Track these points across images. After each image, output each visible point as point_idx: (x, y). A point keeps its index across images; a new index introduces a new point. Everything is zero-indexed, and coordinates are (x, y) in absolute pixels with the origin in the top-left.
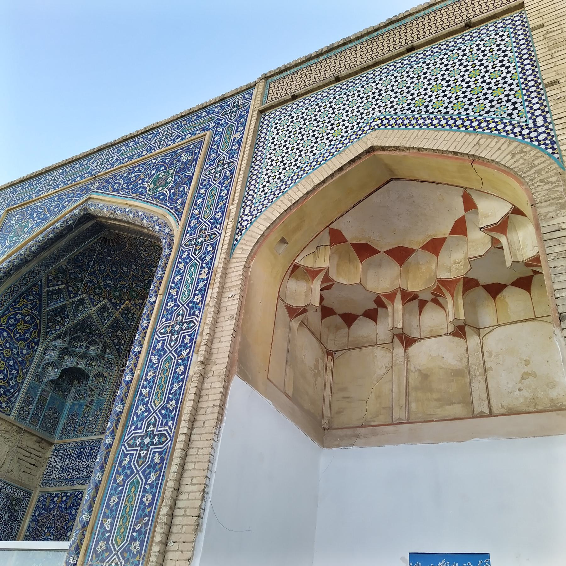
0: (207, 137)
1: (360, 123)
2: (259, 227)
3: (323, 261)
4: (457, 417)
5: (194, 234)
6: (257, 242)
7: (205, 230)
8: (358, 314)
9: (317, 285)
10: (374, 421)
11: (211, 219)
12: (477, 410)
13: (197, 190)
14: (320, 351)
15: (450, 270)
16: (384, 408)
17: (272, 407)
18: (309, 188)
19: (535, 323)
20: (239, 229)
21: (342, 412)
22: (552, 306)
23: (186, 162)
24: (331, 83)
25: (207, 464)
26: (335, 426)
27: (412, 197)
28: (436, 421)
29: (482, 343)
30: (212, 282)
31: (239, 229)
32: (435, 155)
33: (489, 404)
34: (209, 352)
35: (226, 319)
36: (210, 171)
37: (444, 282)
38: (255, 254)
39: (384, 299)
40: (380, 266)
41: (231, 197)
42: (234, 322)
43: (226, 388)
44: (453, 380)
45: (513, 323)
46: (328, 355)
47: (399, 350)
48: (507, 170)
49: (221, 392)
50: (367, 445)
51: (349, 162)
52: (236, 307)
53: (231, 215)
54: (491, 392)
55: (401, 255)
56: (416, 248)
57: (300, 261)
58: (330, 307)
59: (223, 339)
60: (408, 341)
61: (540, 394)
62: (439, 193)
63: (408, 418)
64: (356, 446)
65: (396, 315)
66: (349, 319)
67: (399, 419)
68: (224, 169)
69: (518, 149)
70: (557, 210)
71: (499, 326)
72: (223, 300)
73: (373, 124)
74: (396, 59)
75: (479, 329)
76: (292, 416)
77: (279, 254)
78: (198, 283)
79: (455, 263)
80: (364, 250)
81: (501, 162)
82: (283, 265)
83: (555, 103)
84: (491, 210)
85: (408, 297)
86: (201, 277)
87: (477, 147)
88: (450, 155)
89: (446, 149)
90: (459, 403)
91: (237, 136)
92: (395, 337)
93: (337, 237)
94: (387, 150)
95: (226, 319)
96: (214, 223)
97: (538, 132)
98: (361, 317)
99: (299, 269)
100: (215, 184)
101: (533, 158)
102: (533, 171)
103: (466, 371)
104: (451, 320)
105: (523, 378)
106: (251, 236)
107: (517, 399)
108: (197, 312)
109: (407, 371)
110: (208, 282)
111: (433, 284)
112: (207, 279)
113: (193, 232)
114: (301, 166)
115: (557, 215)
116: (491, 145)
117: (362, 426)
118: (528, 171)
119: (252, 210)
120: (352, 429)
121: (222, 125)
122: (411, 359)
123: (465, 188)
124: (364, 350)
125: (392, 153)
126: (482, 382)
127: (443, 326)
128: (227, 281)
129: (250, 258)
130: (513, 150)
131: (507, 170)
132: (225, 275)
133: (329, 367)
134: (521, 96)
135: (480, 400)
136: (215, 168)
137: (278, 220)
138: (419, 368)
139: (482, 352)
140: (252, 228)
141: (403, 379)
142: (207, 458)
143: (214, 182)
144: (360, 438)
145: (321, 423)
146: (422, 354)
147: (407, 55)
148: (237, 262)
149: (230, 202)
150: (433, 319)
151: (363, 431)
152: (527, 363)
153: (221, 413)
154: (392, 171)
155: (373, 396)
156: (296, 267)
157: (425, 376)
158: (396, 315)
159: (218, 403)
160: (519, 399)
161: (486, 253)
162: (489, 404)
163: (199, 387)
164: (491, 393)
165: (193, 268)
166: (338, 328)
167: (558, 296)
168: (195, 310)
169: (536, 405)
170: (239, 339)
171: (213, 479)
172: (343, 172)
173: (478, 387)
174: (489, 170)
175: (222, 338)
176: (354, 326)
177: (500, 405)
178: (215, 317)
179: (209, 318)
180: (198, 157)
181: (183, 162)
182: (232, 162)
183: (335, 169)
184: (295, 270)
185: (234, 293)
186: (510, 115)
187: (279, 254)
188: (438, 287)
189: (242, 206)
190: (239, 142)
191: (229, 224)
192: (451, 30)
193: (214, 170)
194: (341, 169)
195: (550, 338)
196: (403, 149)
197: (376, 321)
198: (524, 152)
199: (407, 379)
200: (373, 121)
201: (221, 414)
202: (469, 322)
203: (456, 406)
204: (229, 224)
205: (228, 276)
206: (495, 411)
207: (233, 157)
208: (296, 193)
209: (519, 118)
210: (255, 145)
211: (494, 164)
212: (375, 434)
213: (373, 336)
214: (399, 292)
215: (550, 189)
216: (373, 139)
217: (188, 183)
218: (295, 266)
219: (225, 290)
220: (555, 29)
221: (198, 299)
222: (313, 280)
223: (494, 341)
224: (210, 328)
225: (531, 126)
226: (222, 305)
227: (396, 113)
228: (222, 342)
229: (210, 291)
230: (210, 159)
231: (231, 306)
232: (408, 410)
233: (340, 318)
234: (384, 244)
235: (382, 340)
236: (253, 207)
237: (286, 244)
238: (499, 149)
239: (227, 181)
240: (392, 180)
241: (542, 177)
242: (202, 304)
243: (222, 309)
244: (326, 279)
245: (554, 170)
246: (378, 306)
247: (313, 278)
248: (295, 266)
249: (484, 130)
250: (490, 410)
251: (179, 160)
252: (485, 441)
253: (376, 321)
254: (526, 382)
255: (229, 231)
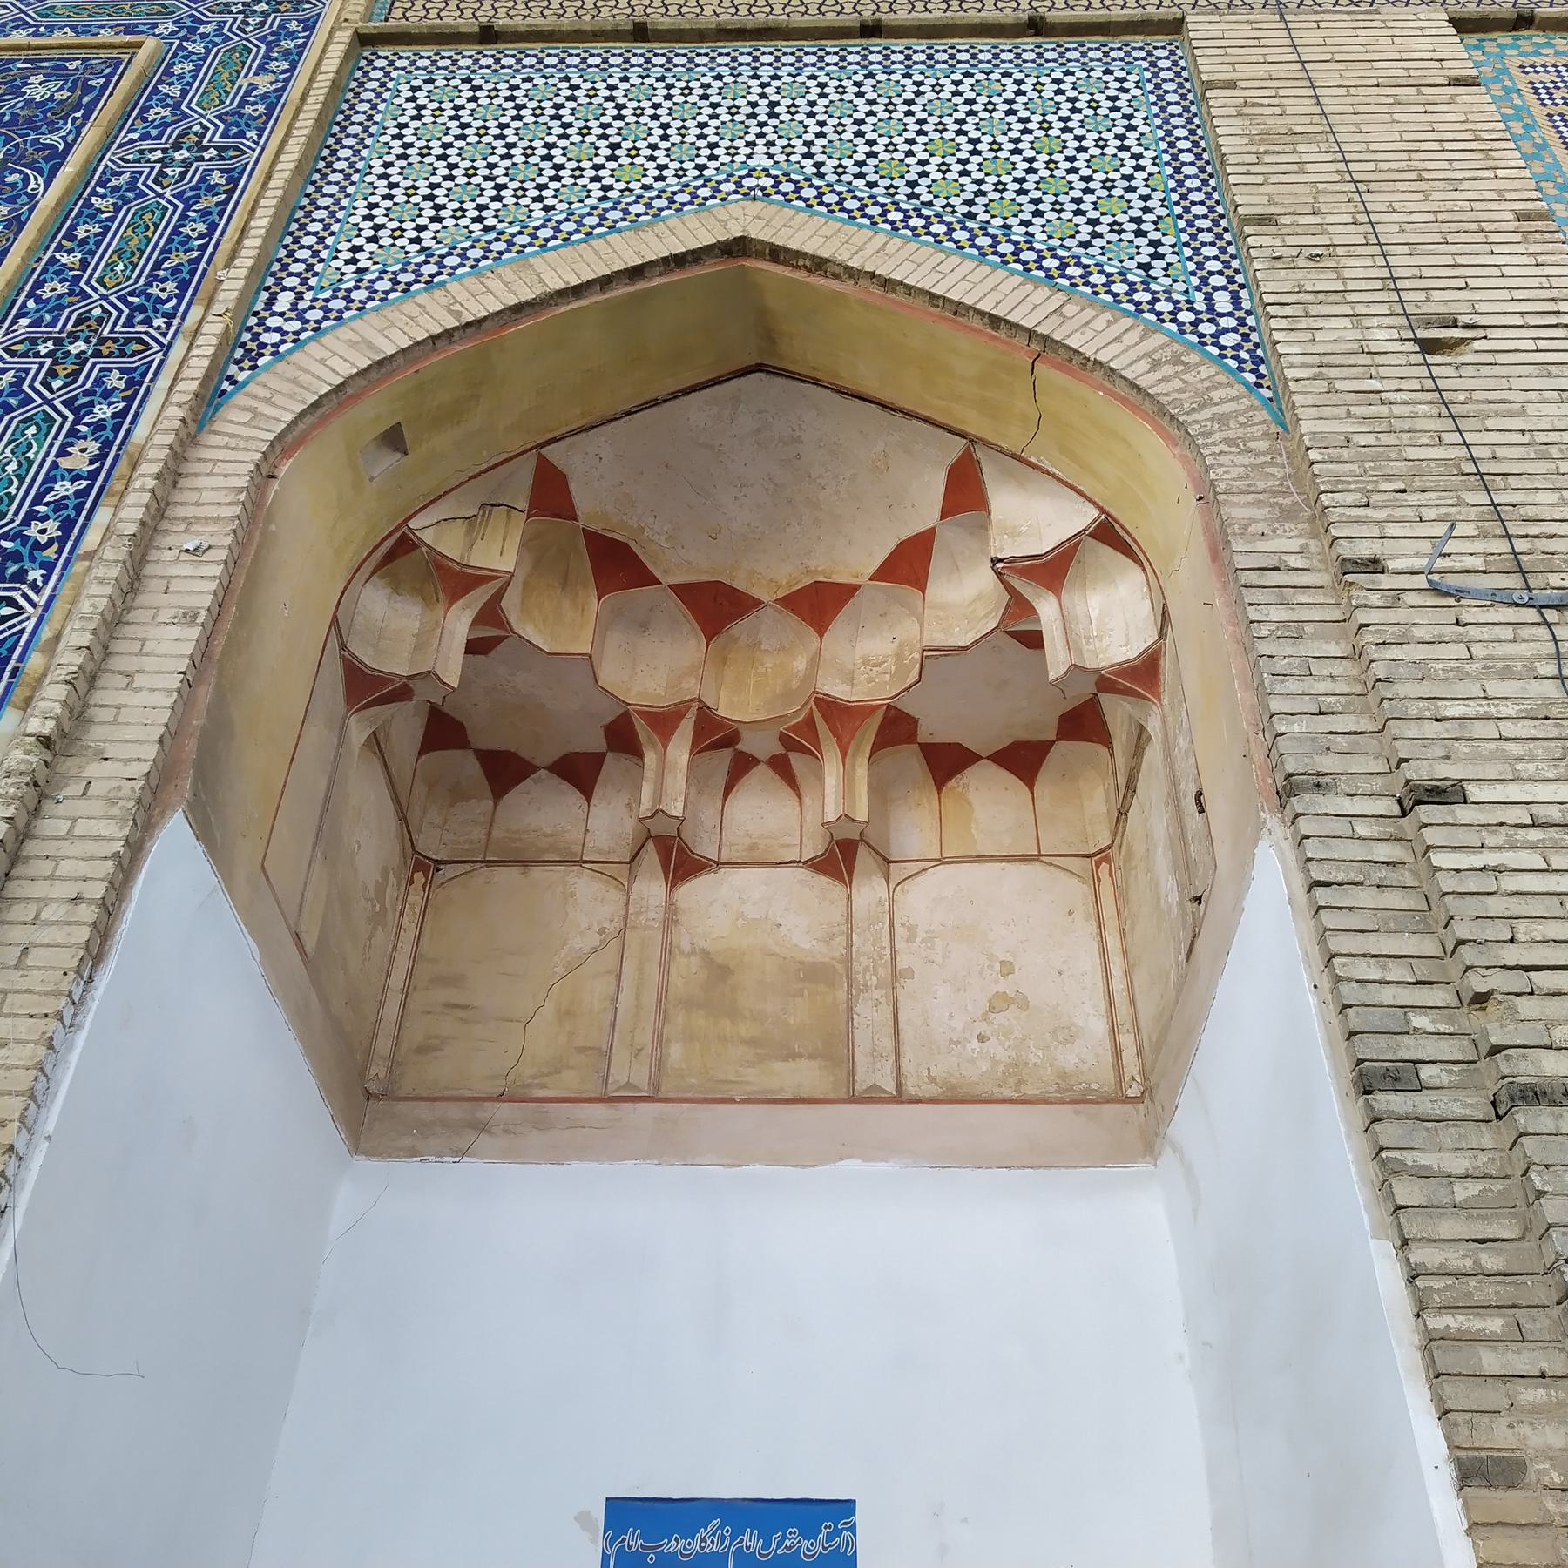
0: (142, 55)
1: (704, 167)
2: (332, 359)
3: (499, 551)
4: (804, 1095)
5: (53, 323)
6: (316, 405)
7: (99, 321)
8: (537, 762)
9: (459, 622)
10: (543, 1086)
11: (131, 294)
12: (863, 1081)
13: (79, 205)
14: (398, 848)
15: (851, 680)
16: (582, 1050)
17: (255, 968)
18: (528, 295)
19: (1035, 868)
20: (243, 349)
21: (436, 1049)
22: (1256, 759)
23: (43, 104)
24: (615, 35)
25: (18, 1103)
26: (406, 1088)
27: (798, 440)
28: (743, 1101)
29: (891, 901)
30: (116, 485)
31: (243, 349)
32: (931, 314)
33: (898, 1069)
34: (77, 715)
35: (160, 619)
36: (141, 152)
37: (831, 708)
38: (300, 441)
39: (641, 727)
40: (644, 627)
41: (226, 246)
42: (195, 632)
43: (135, 849)
44: (801, 990)
45: (980, 859)
46: (416, 870)
47: (651, 888)
48: (1136, 398)
49: (115, 856)
50: (513, 1155)
51: (665, 259)
52: (213, 585)
53: (221, 296)
54: (905, 1036)
55: (716, 608)
56: (765, 596)
57: (424, 527)
58: (459, 717)
59: (139, 681)
60: (682, 863)
61: (1034, 1056)
62: (881, 446)
63: (657, 1087)
64: (474, 1156)
65: (670, 776)
66: (504, 771)
67: (628, 1085)
68: (202, 159)
69: (1168, 352)
70: (1272, 520)
71: (943, 861)
72: (154, 555)
73: (748, 182)
74: (823, 42)
75: (889, 862)
76: (299, 1018)
77: (371, 479)
78: (50, 480)
79: (866, 663)
80: (616, 564)
81: (1124, 373)
82: (364, 530)
83: (1267, 265)
84: (1031, 518)
85: (715, 735)
86: (65, 463)
87: (1055, 319)
88: (976, 322)
89: (968, 301)
90: (812, 1057)
91: (264, 84)
92: (650, 845)
93: (551, 494)
94: (786, 263)
95: (160, 619)
96: (142, 309)
97: (1217, 325)
98: (543, 773)
99: (415, 555)
100: (161, 196)
101: (1206, 384)
102: (1207, 413)
103: (841, 968)
104: (830, 817)
105: (992, 1009)
106: (295, 381)
107: (972, 1061)
108: (35, 574)
109: (668, 949)
110: (94, 488)
111: (794, 710)
112: (93, 475)
113: (48, 318)
114: (500, 226)
115: (1274, 531)
116: (1093, 325)
117: (500, 1098)
118: (1194, 410)
119: (302, 305)
120: (466, 1105)
121: (204, 36)
122: (681, 918)
123: (973, 440)
124: (537, 872)
125: (801, 275)
126: (883, 1006)
127: (787, 840)
128: (178, 497)
129: (278, 449)
130: (1155, 351)
131: (1136, 396)
132: (172, 475)
133: (413, 906)
134: (1172, 231)
135: (875, 1053)
136: (164, 151)
137: (401, 360)
138: (703, 944)
139: (891, 925)
140: (312, 348)
141: (653, 971)
142: (24, 1079)
143: (158, 189)
144: (489, 1132)
145: (362, 1075)
146: (722, 907)
147: (858, 41)
148: (226, 447)
149: (220, 258)
150: (760, 813)
151: (504, 1111)
152: (1007, 969)
153: (102, 927)
154: (773, 342)
155: (549, 1010)
156: (404, 545)
157: (719, 970)
158: (669, 778)
159: (98, 890)
160: (977, 1063)
161: (977, 642)
162: (898, 1069)
163: (21, 823)
164: (903, 1036)
165: (33, 430)
166: (458, 794)
167: (1283, 729)
168: (27, 565)
169: (1020, 1082)
170: (205, 694)
171: (38, 1159)
172: (641, 286)
173: (870, 1017)
174: (1083, 390)
175: (137, 677)
176: (514, 797)
177: (925, 1072)
178: (119, 603)
179: (96, 597)
180: (95, 102)
181: (30, 102)
182: (236, 148)
183: (619, 266)
184: (398, 557)
185: (206, 540)
186: (1146, 267)
187: (371, 479)
188: (810, 722)
189: (266, 278)
190: (272, 102)
191: (208, 327)
192: (991, 21)
193: (159, 154)
194: (636, 273)
195: (1070, 913)
196: (837, 270)
197: (588, 795)
198: (1183, 363)
199: (665, 974)
200: (749, 175)
201: (102, 934)
202: (871, 836)
203: (804, 1064)
204: (208, 327)
205: (183, 483)
206: (911, 1089)
207: (241, 134)
208: (481, 297)
209: (1168, 281)
210: (332, 122)
211: (1098, 374)
212: (543, 1125)
213: (574, 835)
214: (693, 712)
215: (1254, 467)
216: (742, 220)
217: (46, 167)
218: (404, 537)
219: (165, 525)
220: (1266, 101)
221: (43, 531)
222: (451, 603)
223: (929, 899)
224: (94, 632)
225: (1200, 306)
226: (149, 570)
227: (821, 176)
228: (137, 690)
229: (103, 515)
230: (145, 120)
231: (188, 580)
232: (660, 1063)
233: (474, 761)
234: (679, 559)
235: (600, 852)
236: (309, 295)
237: (398, 455)
238: (1117, 339)
239: (214, 197)
240: (758, 368)
241: (1231, 434)
242: (60, 552)
243: (145, 582)
244: (491, 614)
245: (1260, 423)
246: (611, 748)
247: (453, 598)
248: (404, 537)
249: (1075, 285)
250: (899, 1086)
251: (17, 92)
252: (880, 1168)
253: (588, 795)
254: (1000, 1019)
255: (206, 347)
